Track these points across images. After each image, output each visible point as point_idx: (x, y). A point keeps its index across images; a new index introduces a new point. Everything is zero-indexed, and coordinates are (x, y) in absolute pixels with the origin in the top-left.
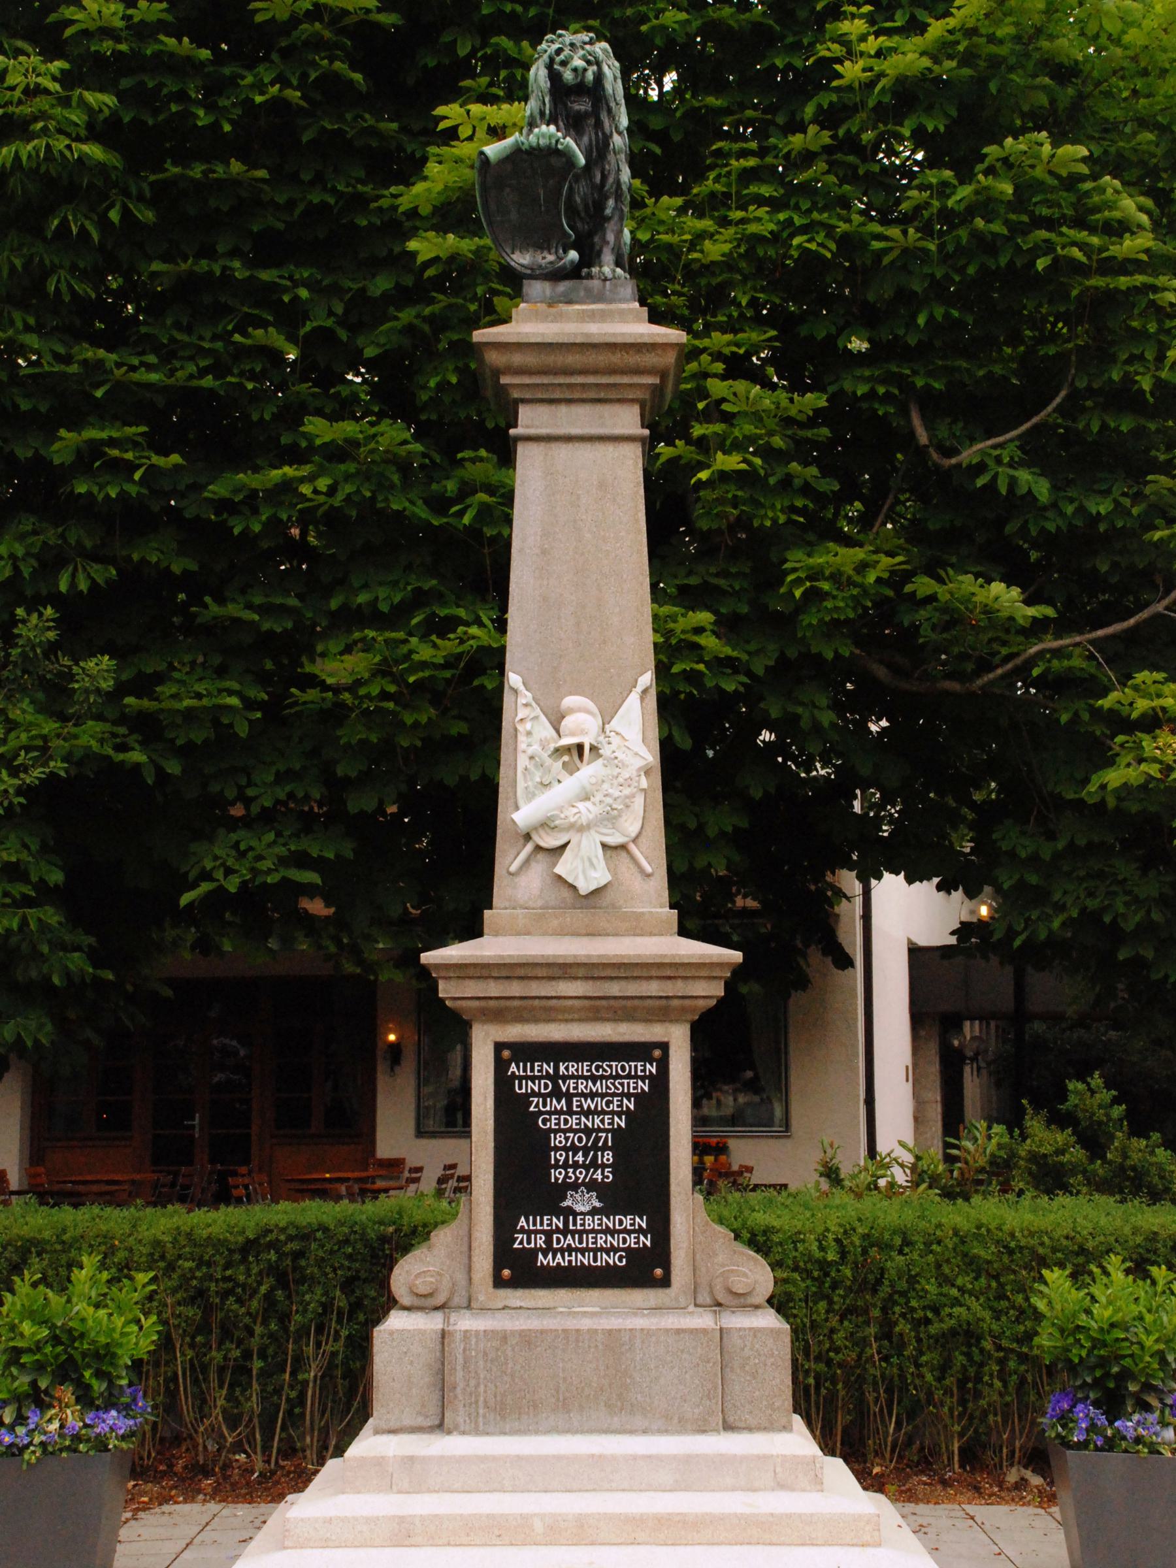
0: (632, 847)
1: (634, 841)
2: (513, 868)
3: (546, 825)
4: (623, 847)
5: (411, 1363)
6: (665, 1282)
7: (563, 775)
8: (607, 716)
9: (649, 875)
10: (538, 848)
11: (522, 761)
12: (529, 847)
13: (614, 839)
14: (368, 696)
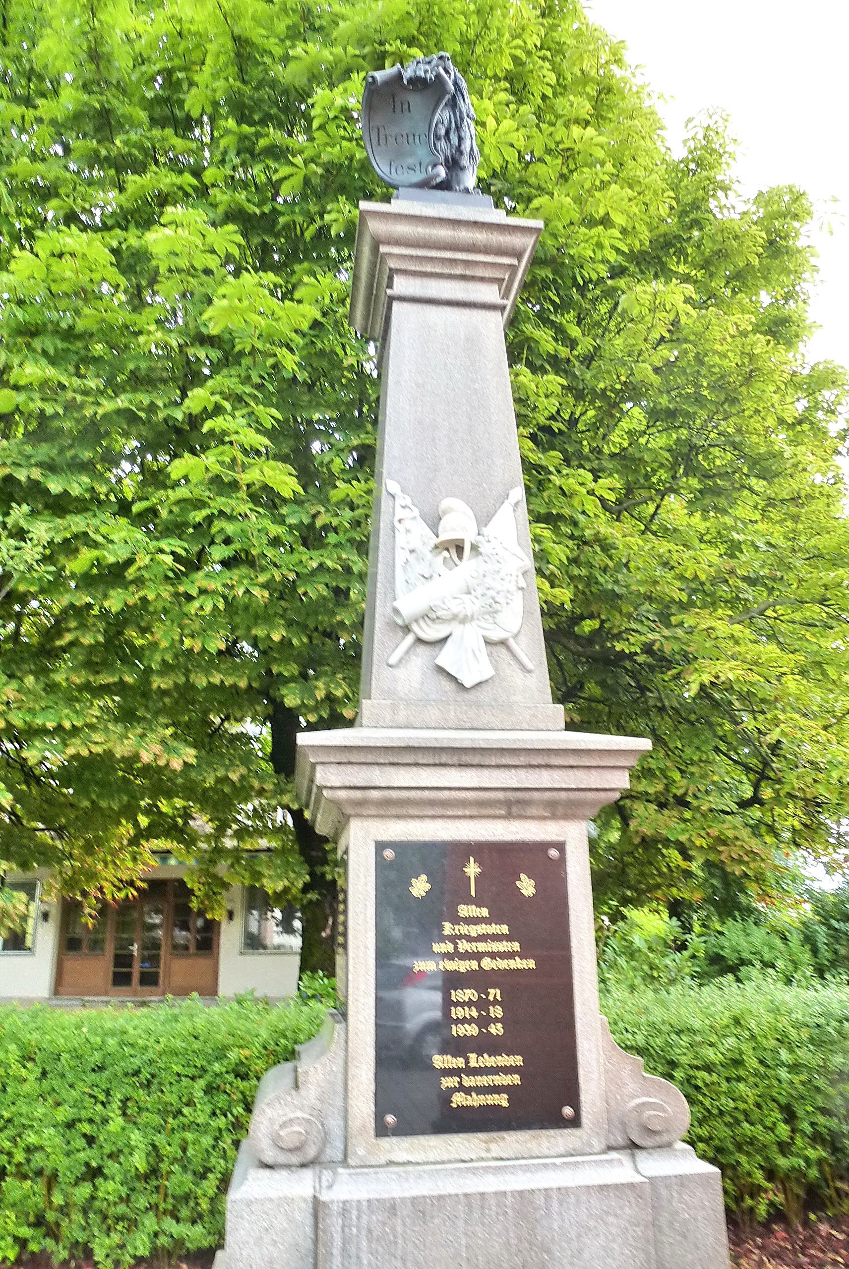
0: (512, 643)
1: (515, 636)
2: (393, 660)
3: (427, 616)
4: (503, 643)
5: (275, 1243)
6: (575, 1122)
7: (443, 570)
8: (483, 520)
9: (529, 671)
10: (419, 641)
11: (401, 556)
12: (410, 639)
13: (496, 635)
14: (175, 166)
